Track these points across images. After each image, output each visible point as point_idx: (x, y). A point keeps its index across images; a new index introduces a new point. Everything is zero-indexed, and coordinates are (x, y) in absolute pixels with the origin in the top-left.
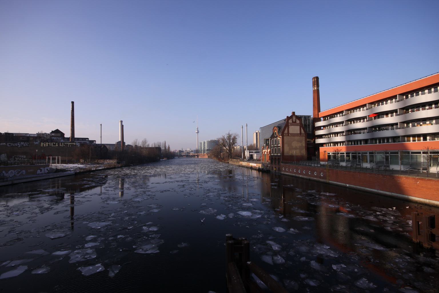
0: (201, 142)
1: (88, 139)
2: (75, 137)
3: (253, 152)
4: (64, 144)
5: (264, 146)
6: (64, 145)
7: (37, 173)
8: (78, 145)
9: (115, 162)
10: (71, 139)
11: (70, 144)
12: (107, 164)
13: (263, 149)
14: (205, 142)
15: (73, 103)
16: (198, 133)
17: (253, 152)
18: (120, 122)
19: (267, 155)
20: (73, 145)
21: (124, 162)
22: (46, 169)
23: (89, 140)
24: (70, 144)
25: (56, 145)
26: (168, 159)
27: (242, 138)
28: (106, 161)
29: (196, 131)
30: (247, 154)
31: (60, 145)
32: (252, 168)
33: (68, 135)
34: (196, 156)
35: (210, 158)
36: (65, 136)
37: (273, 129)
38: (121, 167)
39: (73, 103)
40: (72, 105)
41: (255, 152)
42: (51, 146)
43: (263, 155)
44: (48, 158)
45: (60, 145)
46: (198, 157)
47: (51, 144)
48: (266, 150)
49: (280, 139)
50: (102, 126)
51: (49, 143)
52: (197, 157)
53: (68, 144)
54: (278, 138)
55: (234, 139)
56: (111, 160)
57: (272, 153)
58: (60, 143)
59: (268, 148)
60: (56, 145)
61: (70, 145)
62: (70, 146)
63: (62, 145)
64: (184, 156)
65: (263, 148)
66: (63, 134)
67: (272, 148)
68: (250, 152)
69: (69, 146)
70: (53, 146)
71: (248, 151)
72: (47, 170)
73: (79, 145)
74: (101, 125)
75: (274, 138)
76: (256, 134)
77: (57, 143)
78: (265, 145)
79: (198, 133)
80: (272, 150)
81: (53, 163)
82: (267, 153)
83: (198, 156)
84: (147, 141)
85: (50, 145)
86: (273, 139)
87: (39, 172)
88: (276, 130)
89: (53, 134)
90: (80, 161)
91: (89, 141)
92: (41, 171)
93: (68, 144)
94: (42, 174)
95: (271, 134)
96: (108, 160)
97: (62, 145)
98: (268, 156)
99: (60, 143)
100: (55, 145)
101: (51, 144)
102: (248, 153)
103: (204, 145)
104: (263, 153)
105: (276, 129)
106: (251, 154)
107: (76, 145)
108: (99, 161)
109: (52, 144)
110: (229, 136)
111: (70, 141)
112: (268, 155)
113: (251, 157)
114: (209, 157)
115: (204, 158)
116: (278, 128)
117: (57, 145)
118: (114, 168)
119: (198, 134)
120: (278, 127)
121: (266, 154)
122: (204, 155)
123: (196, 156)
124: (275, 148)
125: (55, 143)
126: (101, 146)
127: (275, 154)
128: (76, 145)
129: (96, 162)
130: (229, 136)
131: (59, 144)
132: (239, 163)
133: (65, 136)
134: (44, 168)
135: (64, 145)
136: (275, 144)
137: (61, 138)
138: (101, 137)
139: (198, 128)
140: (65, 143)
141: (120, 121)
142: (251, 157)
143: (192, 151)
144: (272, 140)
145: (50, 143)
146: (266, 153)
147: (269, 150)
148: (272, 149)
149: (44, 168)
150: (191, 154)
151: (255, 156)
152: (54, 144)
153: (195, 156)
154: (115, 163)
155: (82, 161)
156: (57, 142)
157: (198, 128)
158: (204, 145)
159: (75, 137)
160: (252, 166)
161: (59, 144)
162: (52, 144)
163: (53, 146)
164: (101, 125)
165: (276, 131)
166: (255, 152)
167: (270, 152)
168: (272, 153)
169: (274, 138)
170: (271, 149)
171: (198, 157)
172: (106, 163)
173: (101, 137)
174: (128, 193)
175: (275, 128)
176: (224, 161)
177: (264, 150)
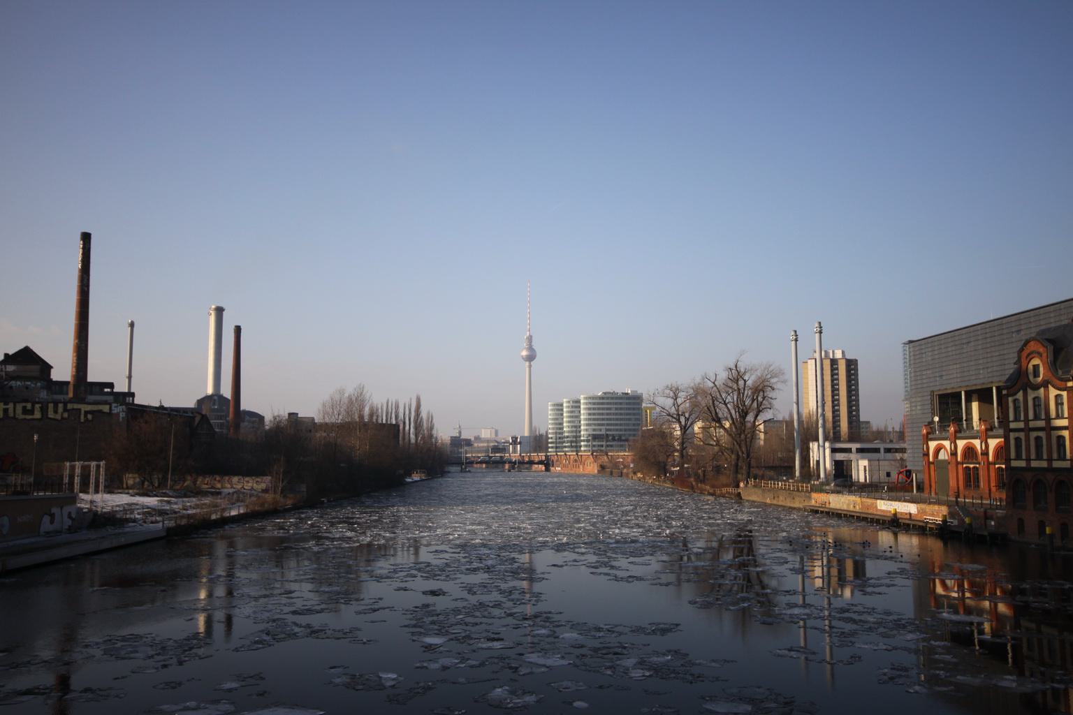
0: (558, 401)
1: (111, 385)
2: (91, 378)
3: (849, 451)
4: (65, 410)
5: (932, 422)
6: (66, 415)
7: (42, 530)
8: (118, 414)
9: (263, 486)
10: (74, 385)
11: (89, 408)
12: (233, 493)
13: (927, 438)
14: (578, 402)
15: (86, 238)
16: (531, 358)
17: (849, 451)
18: (213, 313)
19: (952, 468)
20: (100, 412)
21: (303, 488)
22: (66, 509)
23: (116, 390)
24: (89, 408)
25: (33, 414)
26: (429, 474)
27: (794, 388)
28: (231, 483)
29: (524, 353)
30: (821, 455)
31: (51, 415)
32: (895, 524)
33: (62, 371)
34: (540, 462)
35: (611, 473)
36: (56, 375)
37: (1021, 350)
38: (297, 508)
39: (86, 238)
40: (83, 248)
41: (860, 451)
42: (14, 418)
43: (929, 463)
44: (71, 466)
45: (51, 415)
46: (547, 469)
47: (14, 411)
48: (947, 443)
49: (1065, 394)
50: (135, 329)
51: (6, 404)
52: (542, 467)
53: (80, 410)
54: (1053, 392)
55: (761, 389)
56: (247, 479)
57: (1013, 455)
58: (51, 406)
59: (956, 432)
60: (36, 412)
61: (87, 413)
62: (90, 417)
63: (56, 412)
64: (481, 462)
65: (928, 433)
66: (47, 368)
67: (1012, 435)
68: (834, 451)
69: (86, 416)
70: (24, 417)
71: (827, 444)
72: (70, 516)
73: (122, 415)
74: (132, 325)
75: (1029, 391)
76: (832, 366)
77: (37, 406)
78: (936, 419)
79: (531, 358)
80: (1012, 442)
81: (85, 491)
82: (954, 454)
83: (547, 464)
84: (368, 395)
85: (11, 413)
86: (1020, 395)
87: (46, 525)
88: (1039, 353)
89: (11, 368)
90: (122, 482)
91: (112, 393)
92: (52, 522)
93: (80, 410)
94: (58, 532)
95: (1010, 369)
96: (235, 479)
97: (56, 412)
98: (993, 474)
99: (51, 406)
100: (32, 412)
101: (14, 411)
102: (828, 452)
103: (575, 416)
104: (927, 455)
105: (1041, 350)
106: (840, 456)
107: (110, 414)
108: (198, 483)
109: (19, 407)
110: (737, 376)
111: (71, 395)
112: (957, 463)
113: (842, 474)
114: (602, 467)
115: (579, 476)
116: (1051, 348)
117: (37, 415)
118: (275, 512)
119: (530, 366)
120: (1049, 341)
121: (946, 462)
122: (579, 461)
123: (540, 462)
124: (1034, 435)
125: (29, 406)
126: (194, 418)
127: (1034, 464)
128: (110, 414)
129: (186, 484)
130: (737, 376)
131: (44, 410)
132: (810, 498)
133: (56, 375)
134: (62, 508)
135: (66, 415)
136: (1031, 416)
137: (39, 384)
138: (130, 377)
139: (530, 339)
140: (70, 406)
141: (213, 307)
142: (842, 474)
143: (515, 441)
144: (1015, 401)
145: (11, 406)
146: (943, 456)
147: (993, 443)
148: (1018, 440)
149: (61, 509)
150: (515, 454)
151: (861, 469)
152: (25, 411)
153: (531, 463)
154: (265, 491)
155: (130, 479)
156: (38, 403)
157: (530, 339)
158: (575, 416)
159: (91, 378)
160: (899, 516)
161: (44, 410)
162: (19, 407)
163: (24, 417)
164: (132, 325)
165: (1036, 361)
166: (860, 451)
167: (1002, 452)
168: (1013, 455)
169: (1029, 391)
170: (1007, 438)
171: (547, 469)
172: (231, 491)
173: (130, 377)
174: (561, 613)
175: (1033, 346)
176: (713, 486)
177: (933, 445)
